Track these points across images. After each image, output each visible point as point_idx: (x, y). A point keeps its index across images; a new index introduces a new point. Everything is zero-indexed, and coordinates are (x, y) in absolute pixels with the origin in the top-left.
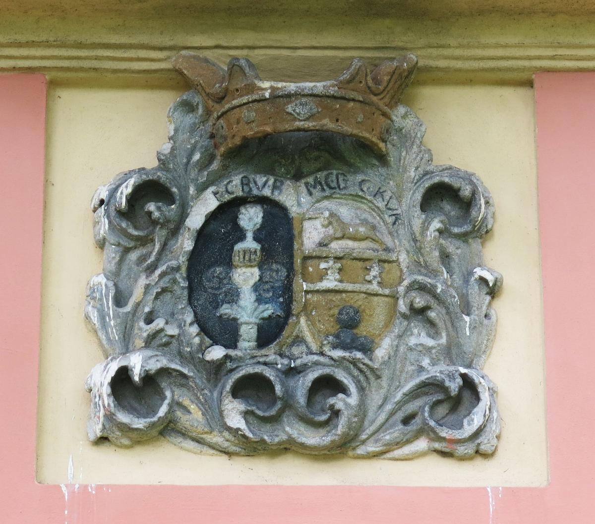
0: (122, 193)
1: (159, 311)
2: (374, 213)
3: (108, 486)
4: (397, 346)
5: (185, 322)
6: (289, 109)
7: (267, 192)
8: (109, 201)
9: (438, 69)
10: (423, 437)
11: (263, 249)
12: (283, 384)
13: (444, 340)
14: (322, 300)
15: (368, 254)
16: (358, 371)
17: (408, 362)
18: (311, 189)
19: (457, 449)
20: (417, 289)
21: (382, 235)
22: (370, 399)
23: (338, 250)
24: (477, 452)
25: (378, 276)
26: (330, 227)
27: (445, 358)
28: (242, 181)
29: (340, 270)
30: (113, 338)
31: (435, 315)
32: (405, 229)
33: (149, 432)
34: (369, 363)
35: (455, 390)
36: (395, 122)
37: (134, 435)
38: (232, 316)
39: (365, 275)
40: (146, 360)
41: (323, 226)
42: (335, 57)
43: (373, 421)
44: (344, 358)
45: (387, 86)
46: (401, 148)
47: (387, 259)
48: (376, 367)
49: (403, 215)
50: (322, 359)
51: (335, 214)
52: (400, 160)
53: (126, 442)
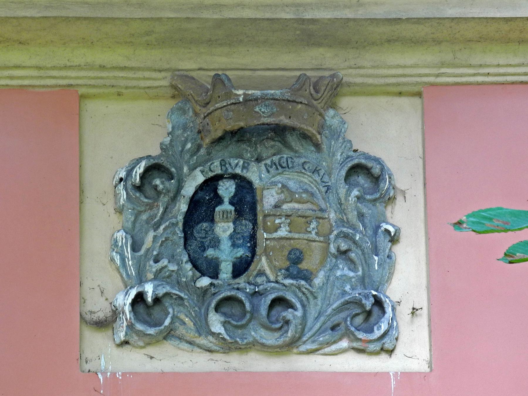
0: (136, 172)
1: (164, 254)
2: (312, 185)
3: (130, 373)
4: (328, 277)
5: (182, 261)
6: (257, 109)
7: (238, 171)
8: (126, 179)
9: (355, 84)
10: (345, 339)
11: (236, 210)
12: (251, 303)
13: (360, 273)
14: (277, 245)
15: (309, 213)
16: (302, 293)
17: (335, 288)
18: (269, 168)
19: (368, 347)
20: (342, 237)
21: (318, 200)
22: (309, 313)
23: (288, 210)
24: (382, 349)
25: (316, 228)
26: (282, 195)
27: (361, 285)
28: (221, 163)
29: (289, 224)
30: (131, 273)
31: (354, 255)
32: (333, 196)
33: (157, 337)
34: (310, 288)
35: (369, 306)
36: (327, 121)
37: (147, 340)
38: (215, 256)
39: (307, 228)
40: (155, 288)
41: (278, 194)
42: (283, 76)
43: (311, 329)
44: (292, 284)
45: (323, 94)
46: (331, 139)
47: (321, 216)
48: (314, 291)
49: (332, 186)
50: (277, 285)
51: (286, 186)
52: (330, 148)
53: (141, 344)
